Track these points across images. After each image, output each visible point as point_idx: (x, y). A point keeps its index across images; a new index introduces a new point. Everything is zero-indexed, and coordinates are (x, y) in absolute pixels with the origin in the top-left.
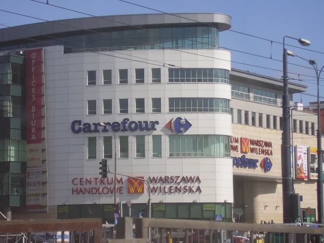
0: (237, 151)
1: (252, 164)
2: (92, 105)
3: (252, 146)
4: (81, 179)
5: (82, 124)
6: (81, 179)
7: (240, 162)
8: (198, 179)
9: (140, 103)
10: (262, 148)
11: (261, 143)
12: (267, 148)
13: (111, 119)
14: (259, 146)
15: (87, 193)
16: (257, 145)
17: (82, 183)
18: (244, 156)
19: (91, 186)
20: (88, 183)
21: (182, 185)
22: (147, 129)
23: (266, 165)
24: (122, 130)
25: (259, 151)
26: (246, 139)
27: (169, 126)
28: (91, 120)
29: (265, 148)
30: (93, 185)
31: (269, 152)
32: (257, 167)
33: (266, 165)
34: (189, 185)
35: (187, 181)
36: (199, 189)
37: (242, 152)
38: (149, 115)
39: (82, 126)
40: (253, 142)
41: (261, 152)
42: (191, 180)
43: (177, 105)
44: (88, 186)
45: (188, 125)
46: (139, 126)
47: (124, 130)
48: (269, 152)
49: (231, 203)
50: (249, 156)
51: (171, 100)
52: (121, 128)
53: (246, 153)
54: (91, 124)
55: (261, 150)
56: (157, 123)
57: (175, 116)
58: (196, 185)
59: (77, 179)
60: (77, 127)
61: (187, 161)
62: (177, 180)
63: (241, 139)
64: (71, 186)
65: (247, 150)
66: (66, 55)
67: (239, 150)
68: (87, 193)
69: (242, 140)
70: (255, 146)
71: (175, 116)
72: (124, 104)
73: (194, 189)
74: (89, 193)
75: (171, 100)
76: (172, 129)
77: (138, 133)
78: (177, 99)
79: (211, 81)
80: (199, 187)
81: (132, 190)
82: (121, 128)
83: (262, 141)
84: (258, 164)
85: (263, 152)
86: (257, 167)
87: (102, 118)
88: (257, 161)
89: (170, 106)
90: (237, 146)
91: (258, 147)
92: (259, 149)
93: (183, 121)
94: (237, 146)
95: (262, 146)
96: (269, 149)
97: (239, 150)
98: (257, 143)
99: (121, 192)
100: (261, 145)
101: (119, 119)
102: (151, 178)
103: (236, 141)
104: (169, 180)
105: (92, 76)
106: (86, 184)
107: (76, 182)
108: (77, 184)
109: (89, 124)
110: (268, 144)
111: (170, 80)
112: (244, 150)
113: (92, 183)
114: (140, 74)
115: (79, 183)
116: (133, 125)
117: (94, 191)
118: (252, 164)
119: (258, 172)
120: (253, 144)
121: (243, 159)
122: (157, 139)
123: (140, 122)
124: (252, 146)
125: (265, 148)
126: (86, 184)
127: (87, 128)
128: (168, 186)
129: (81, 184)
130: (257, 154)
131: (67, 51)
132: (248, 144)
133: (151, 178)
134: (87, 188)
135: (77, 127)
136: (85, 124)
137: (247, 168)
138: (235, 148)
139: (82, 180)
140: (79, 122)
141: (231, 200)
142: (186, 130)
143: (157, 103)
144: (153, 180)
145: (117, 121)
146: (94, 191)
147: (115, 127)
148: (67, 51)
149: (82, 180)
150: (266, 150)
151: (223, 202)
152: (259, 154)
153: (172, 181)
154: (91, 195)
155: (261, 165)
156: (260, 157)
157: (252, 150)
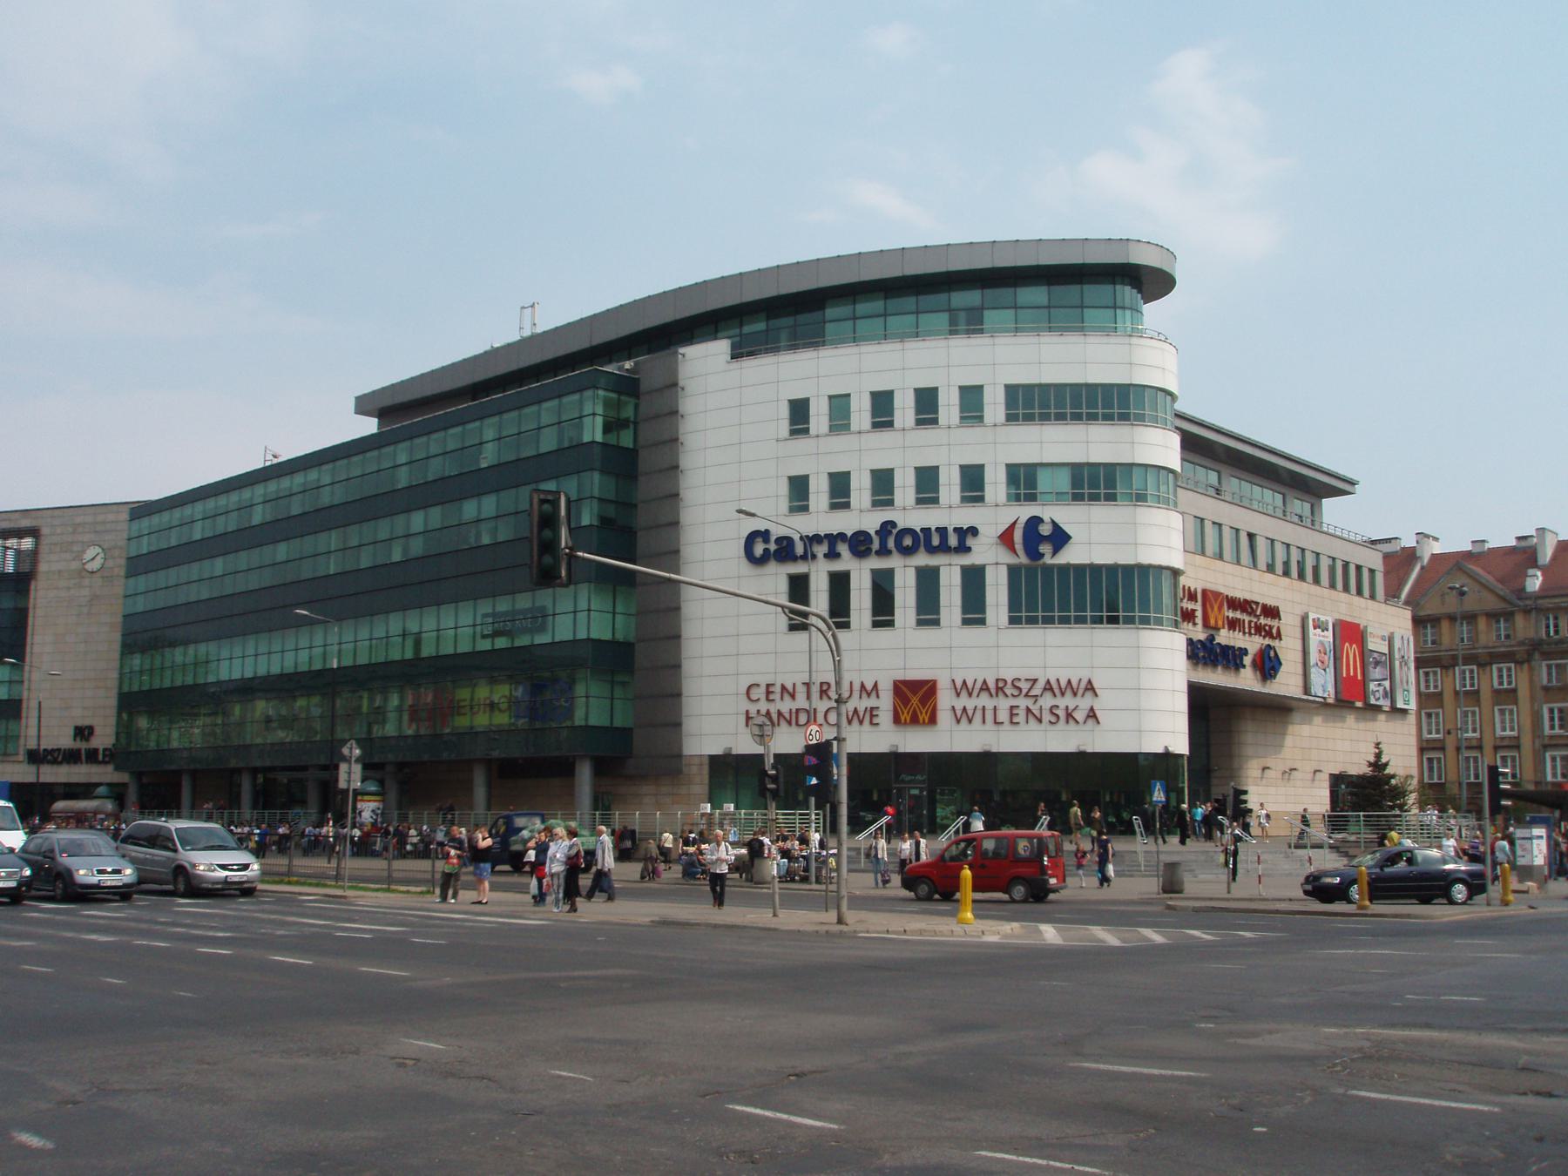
0: (1195, 624)
1: (1230, 658)
2: (799, 488)
3: (1231, 614)
4: (768, 686)
5: (773, 538)
6: (768, 686)
7: (1202, 653)
8: (1090, 687)
9: (927, 480)
10: (1255, 620)
11: (1254, 607)
12: (1269, 621)
13: (846, 523)
14: (1249, 614)
15: (783, 724)
16: (1244, 610)
17: (771, 697)
18: (1211, 638)
19: (794, 706)
20: (786, 697)
21: (1047, 701)
22: (944, 548)
23: (1267, 667)
24: (878, 553)
25: (1250, 628)
26: (1217, 595)
27: (1006, 538)
28: (800, 526)
29: (1263, 621)
30: (801, 701)
31: (1274, 631)
32: (1244, 666)
33: (1268, 665)
34: (1067, 701)
35: (1057, 691)
36: (1092, 715)
37: (1206, 625)
38: (950, 513)
39: (773, 547)
40: (1234, 604)
41: (1253, 631)
42: (1070, 688)
43: (1029, 404)
44: (786, 706)
45: (1060, 538)
46: (920, 541)
47: (884, 552)
48: (1274, 631)
49: (1182, 756)
50: (1225, 637)
51: (1012, 391)
52: (876, 545)
53: (1217, 629)
54: (796, 537)
55: (1253, 625)
56: (973, 531)
57: (1025, 512)
58: (1084, 703)
59: (758, 685)
60: (759, 549)
61: (1056, 636)
62: (1030, 690)
63: (1204, 592)
64: (745, 705)
65: (1220, 623)
66: (736, 365)
67: (1199, 620)
68: (783, 724)
69: (1209, 597)
70: (1238, 615)
71: (1025, 512)
72: (883, 482)
73: (1079, 716)
74: (790, 723)
75: (1012, 391)
76: (1016, 546)
77: (923, 559)
78: (1029, 389)
79: (1124, 417)
80: (1092, 709)
81: (905, 716)
82: (876, 545)
83: (1257, 603)
84: (1247, 660)
85: (1259, 630)
86: (1244, 666)
87: (821, 519)
88: (1244, 652)
89: (1011, 609)
90: (1194, 611)
91: (1246, 618)
92: (1250, 622)
93: (1045, 530)
94: (1194, 611)
95: (1256, 616)
96: (1275, 623)
97: (1199, 620)
98: (1244, 606)
99: (875, 721)
100: (1252, 613)
101: (871, 522)
102: (959, 684)
103: (1192, 597)
104: (1009, 690)
105: (799, 412)
106: (782, 699)
107: (759, 693)
108: (758, 699)
109: (789, 540)
110: (1272, 612)
111: (1014, 621)
112: (1212, 622)
113: (798, 696)
114: (927, 402)
115: (763, 697)
116: (908, 541)
117: (803, 718)
118: (1230, 658)
119: (1246, 680)
120: (1235, 609)
121: (1208, 644)
122: (974, 580)
123: (926, 531)
124: (1231, 614)
125: (1263, 621)
126: (782, 699)
127: (784, 551)
128: (1004, 704)
129: (768, 699)
130: (1244, 633)
131: (736, 355)
132: (1220, 608)
133: (959, 684)
134: (785, 710)
135: (759, 549)
136: (779, 540)
137: (1220, 668)
138: (1188, 616)
139: (771, 689)
140: (765, 535)
141: (1181, 746)
142: (1056, 551)
143: (973, 480)
144: (962, 689)
145: (863, 528)
146: (803, 718)
147: (860, 544)
148: (736, 355)
149: (771, 689)
150: (1266, 625)
151: (1161, 750)
152: (1250, 634)
153: (1016, 693)
154: (794, 728)
155: (1254, 664)
156: (1252, 644)
157: (1233, 624)
